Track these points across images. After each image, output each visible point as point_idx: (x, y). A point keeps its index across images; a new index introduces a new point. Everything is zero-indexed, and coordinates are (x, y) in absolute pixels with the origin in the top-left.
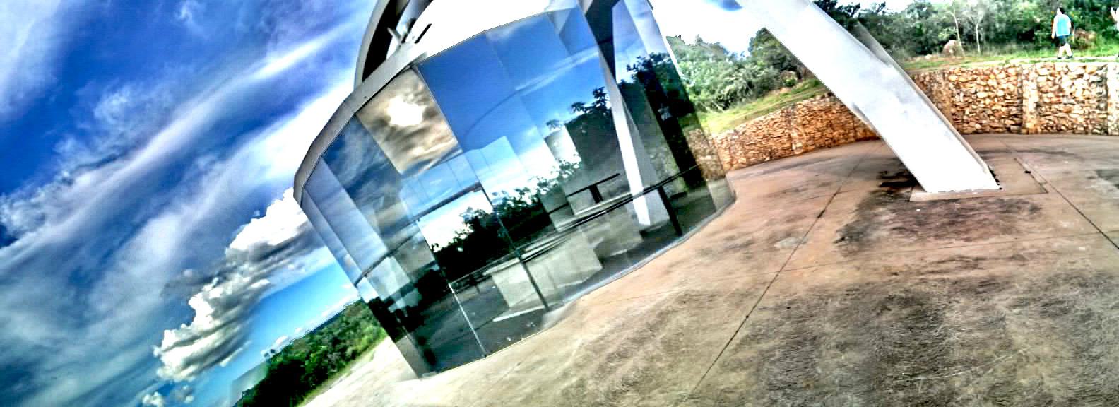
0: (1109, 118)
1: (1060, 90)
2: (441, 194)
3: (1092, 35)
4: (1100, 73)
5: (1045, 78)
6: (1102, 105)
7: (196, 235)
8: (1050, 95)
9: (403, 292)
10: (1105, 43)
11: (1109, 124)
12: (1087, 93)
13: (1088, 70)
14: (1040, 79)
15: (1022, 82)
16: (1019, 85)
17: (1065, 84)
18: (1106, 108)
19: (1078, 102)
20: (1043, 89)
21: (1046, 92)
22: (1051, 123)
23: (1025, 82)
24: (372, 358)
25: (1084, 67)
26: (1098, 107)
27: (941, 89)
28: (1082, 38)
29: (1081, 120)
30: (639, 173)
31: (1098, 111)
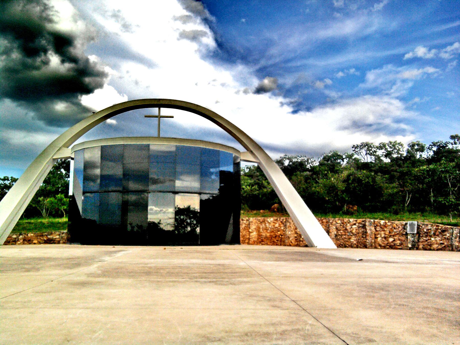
0: (367, 241)
1: (346, 229)
2: (94, 277)
3: (355, 208)
4: (363, 223)
5: (339, 225)
6: (364, 236)
7: (115, 277)
8: (341, 231)
9: (255, 238)
10: (363, 212)
11: (368, 244)
12: (357, 231)
13: (358, 221)
14: (337, 225)
15: (329, 225)
16: (328, 226)
17: (348, 227)
18: (366, 237)
19: (354, 235)
20: (339, 229)
21: (340, 230)
22: (342, 243)
23: (331, 225)
24: (165, 249)
25: (356, 221)
26: (363, 237)
27: (291, 226)
28: (350, 209)
29: (355, 242)
30: (233, 123)
31: (362, 239)
